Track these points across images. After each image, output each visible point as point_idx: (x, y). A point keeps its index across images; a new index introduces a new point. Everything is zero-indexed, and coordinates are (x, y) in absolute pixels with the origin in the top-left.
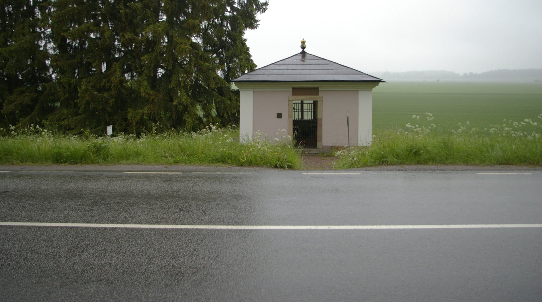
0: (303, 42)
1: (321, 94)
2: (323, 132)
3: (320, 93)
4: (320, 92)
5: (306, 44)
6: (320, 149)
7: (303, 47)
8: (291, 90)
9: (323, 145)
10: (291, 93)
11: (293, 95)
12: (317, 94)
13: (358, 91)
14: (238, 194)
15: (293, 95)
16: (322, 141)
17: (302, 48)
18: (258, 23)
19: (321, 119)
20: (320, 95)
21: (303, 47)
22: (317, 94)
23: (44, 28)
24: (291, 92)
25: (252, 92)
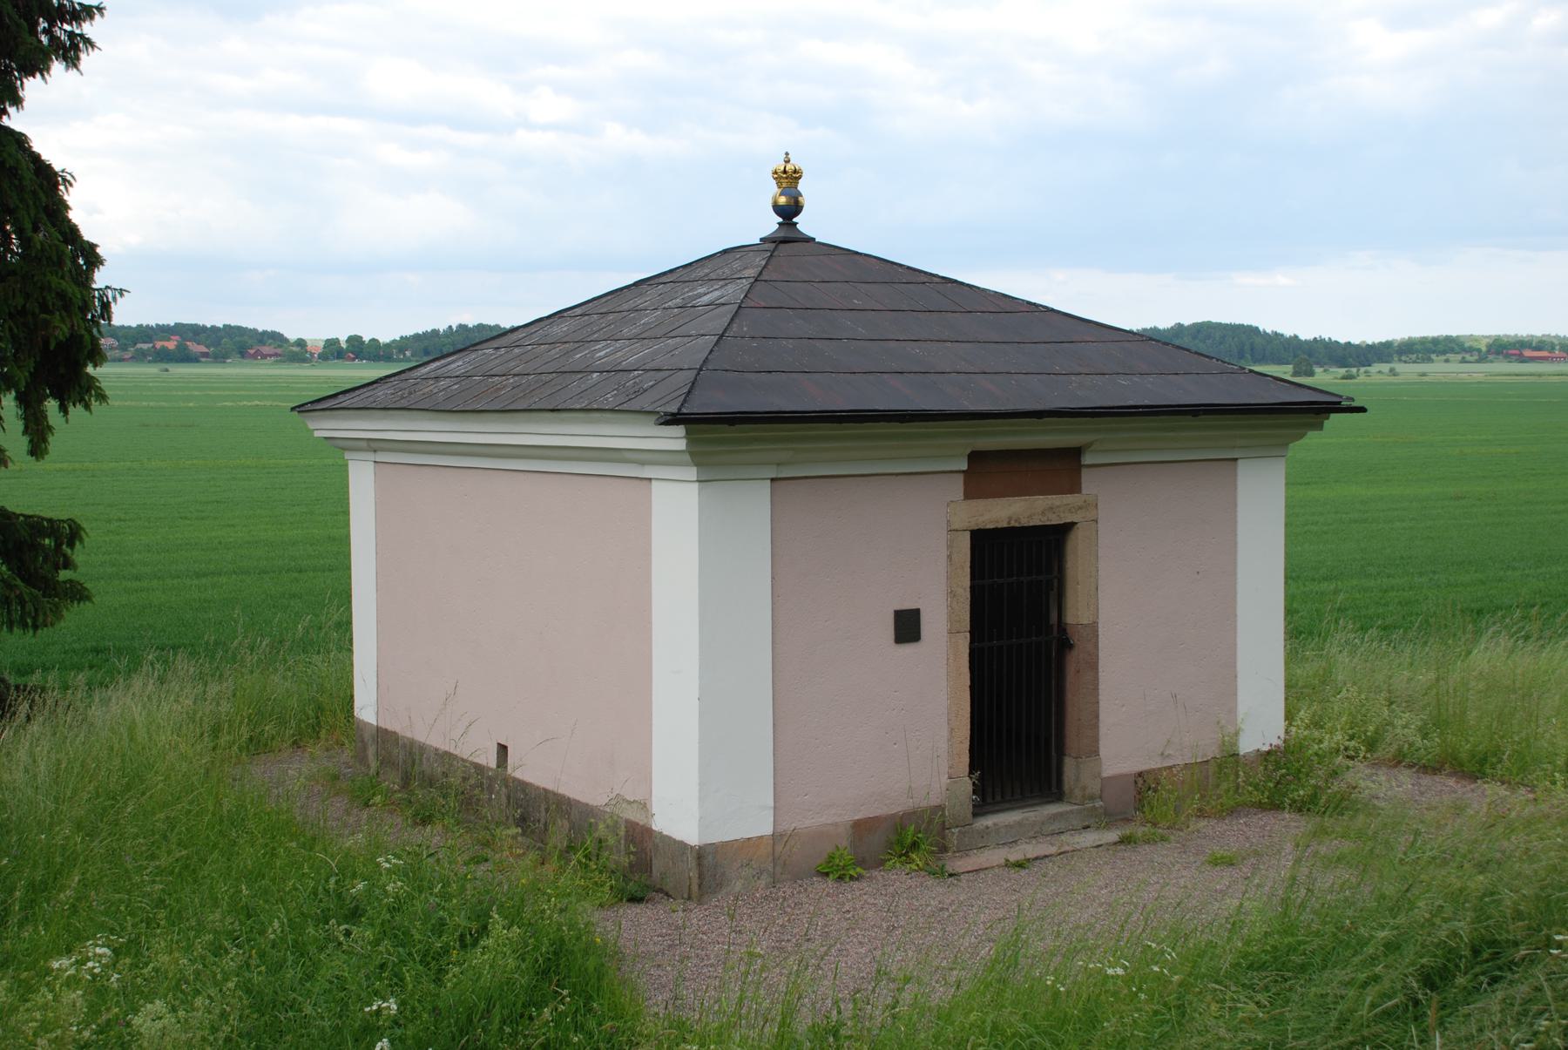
0: (789, 178)
1: (1089, 482)
2: (1283, 674)
3: (1086, 475)
4: (1084, 472)
5: (802, 186)
6: (1092, 798)
7: (789, 211)
8: (964, 467)
9: (1105, 775)
10: (957, 486)
11: (969, 494)
12: (1075, 488)
13: (1236, 459)
14: (1513, 790)
15: (969, 494)
16: (1096, 752)
17: (778, 209)
18: (87, 29)
19: (1093, 628)
20: (1084, 491)
21: (789, 211)
22: (1075, 488)
23: (1413, 354)
24: (960, 479)
25: (769, 481)
